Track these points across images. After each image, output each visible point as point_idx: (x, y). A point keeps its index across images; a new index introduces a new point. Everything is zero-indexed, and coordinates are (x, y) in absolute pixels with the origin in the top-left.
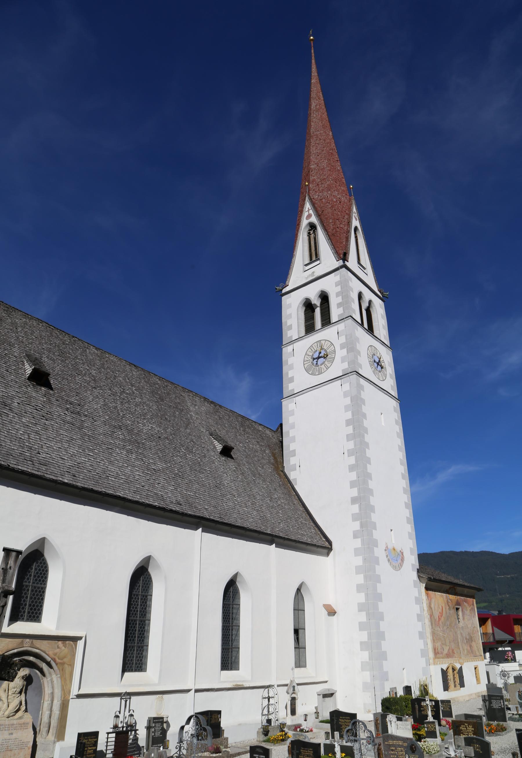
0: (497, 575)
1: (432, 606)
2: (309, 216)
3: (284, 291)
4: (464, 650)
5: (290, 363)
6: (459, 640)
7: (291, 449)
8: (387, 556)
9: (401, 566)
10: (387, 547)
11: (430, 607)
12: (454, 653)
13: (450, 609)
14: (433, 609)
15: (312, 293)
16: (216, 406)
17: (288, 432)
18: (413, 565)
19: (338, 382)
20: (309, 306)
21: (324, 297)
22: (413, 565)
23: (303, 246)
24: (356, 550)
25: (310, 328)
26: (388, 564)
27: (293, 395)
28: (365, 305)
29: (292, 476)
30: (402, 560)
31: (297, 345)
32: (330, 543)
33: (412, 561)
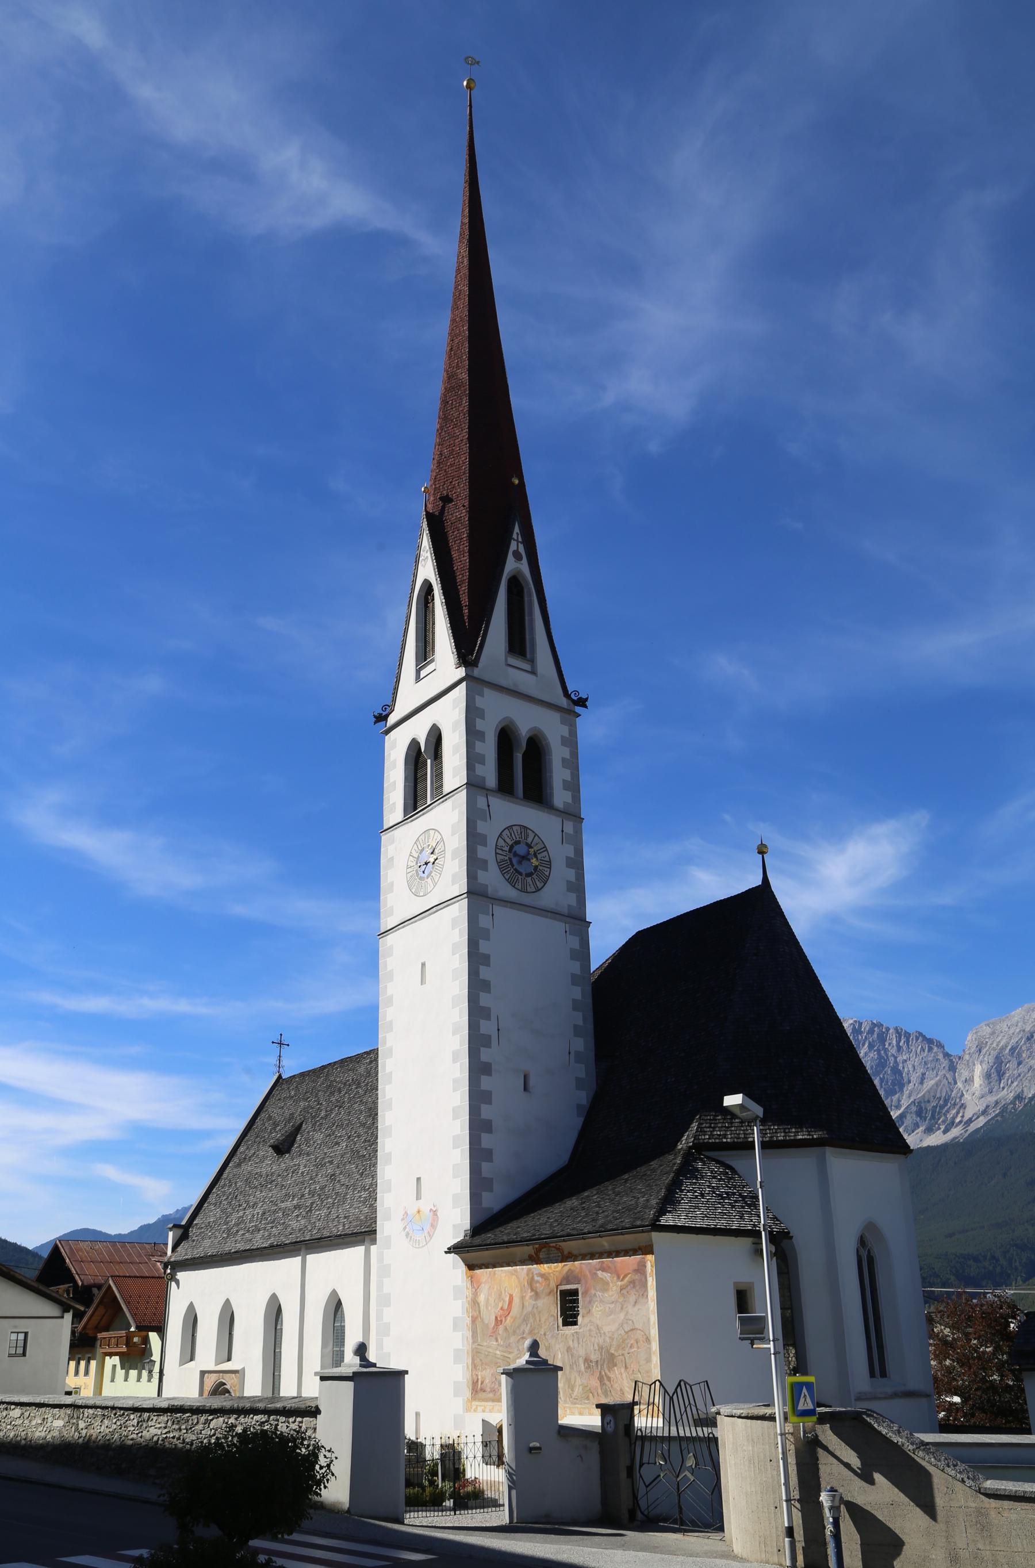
1: (482, 1298)
3: (392, 719)
13: (537, 1295)
15: (418, 729)
21: (436, 737)
30: (433, 1226)
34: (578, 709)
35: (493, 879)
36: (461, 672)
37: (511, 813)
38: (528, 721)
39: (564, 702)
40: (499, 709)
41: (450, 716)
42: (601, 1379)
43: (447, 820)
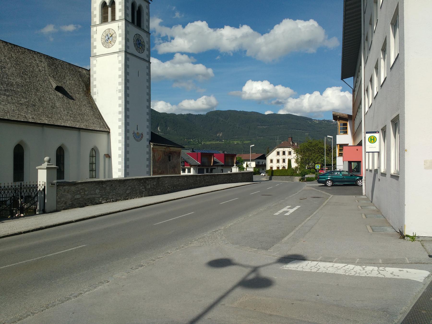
0: (259, 126)
1: (155, 155)
5: (94, 37)
7: (94, 84)
9: (141, 140)
11: (154, 156)
16: (53, 60)
19: (116, 55)
24: (119, 133)
25: (104, 19)
27: (95, 56)
28: (137, 9)
29: (94, 97)
30: (142, 137)
32: (109, 129)
33: (147, 137)
35: (133, 50)
37: (135, 30)
43: (118, 27)
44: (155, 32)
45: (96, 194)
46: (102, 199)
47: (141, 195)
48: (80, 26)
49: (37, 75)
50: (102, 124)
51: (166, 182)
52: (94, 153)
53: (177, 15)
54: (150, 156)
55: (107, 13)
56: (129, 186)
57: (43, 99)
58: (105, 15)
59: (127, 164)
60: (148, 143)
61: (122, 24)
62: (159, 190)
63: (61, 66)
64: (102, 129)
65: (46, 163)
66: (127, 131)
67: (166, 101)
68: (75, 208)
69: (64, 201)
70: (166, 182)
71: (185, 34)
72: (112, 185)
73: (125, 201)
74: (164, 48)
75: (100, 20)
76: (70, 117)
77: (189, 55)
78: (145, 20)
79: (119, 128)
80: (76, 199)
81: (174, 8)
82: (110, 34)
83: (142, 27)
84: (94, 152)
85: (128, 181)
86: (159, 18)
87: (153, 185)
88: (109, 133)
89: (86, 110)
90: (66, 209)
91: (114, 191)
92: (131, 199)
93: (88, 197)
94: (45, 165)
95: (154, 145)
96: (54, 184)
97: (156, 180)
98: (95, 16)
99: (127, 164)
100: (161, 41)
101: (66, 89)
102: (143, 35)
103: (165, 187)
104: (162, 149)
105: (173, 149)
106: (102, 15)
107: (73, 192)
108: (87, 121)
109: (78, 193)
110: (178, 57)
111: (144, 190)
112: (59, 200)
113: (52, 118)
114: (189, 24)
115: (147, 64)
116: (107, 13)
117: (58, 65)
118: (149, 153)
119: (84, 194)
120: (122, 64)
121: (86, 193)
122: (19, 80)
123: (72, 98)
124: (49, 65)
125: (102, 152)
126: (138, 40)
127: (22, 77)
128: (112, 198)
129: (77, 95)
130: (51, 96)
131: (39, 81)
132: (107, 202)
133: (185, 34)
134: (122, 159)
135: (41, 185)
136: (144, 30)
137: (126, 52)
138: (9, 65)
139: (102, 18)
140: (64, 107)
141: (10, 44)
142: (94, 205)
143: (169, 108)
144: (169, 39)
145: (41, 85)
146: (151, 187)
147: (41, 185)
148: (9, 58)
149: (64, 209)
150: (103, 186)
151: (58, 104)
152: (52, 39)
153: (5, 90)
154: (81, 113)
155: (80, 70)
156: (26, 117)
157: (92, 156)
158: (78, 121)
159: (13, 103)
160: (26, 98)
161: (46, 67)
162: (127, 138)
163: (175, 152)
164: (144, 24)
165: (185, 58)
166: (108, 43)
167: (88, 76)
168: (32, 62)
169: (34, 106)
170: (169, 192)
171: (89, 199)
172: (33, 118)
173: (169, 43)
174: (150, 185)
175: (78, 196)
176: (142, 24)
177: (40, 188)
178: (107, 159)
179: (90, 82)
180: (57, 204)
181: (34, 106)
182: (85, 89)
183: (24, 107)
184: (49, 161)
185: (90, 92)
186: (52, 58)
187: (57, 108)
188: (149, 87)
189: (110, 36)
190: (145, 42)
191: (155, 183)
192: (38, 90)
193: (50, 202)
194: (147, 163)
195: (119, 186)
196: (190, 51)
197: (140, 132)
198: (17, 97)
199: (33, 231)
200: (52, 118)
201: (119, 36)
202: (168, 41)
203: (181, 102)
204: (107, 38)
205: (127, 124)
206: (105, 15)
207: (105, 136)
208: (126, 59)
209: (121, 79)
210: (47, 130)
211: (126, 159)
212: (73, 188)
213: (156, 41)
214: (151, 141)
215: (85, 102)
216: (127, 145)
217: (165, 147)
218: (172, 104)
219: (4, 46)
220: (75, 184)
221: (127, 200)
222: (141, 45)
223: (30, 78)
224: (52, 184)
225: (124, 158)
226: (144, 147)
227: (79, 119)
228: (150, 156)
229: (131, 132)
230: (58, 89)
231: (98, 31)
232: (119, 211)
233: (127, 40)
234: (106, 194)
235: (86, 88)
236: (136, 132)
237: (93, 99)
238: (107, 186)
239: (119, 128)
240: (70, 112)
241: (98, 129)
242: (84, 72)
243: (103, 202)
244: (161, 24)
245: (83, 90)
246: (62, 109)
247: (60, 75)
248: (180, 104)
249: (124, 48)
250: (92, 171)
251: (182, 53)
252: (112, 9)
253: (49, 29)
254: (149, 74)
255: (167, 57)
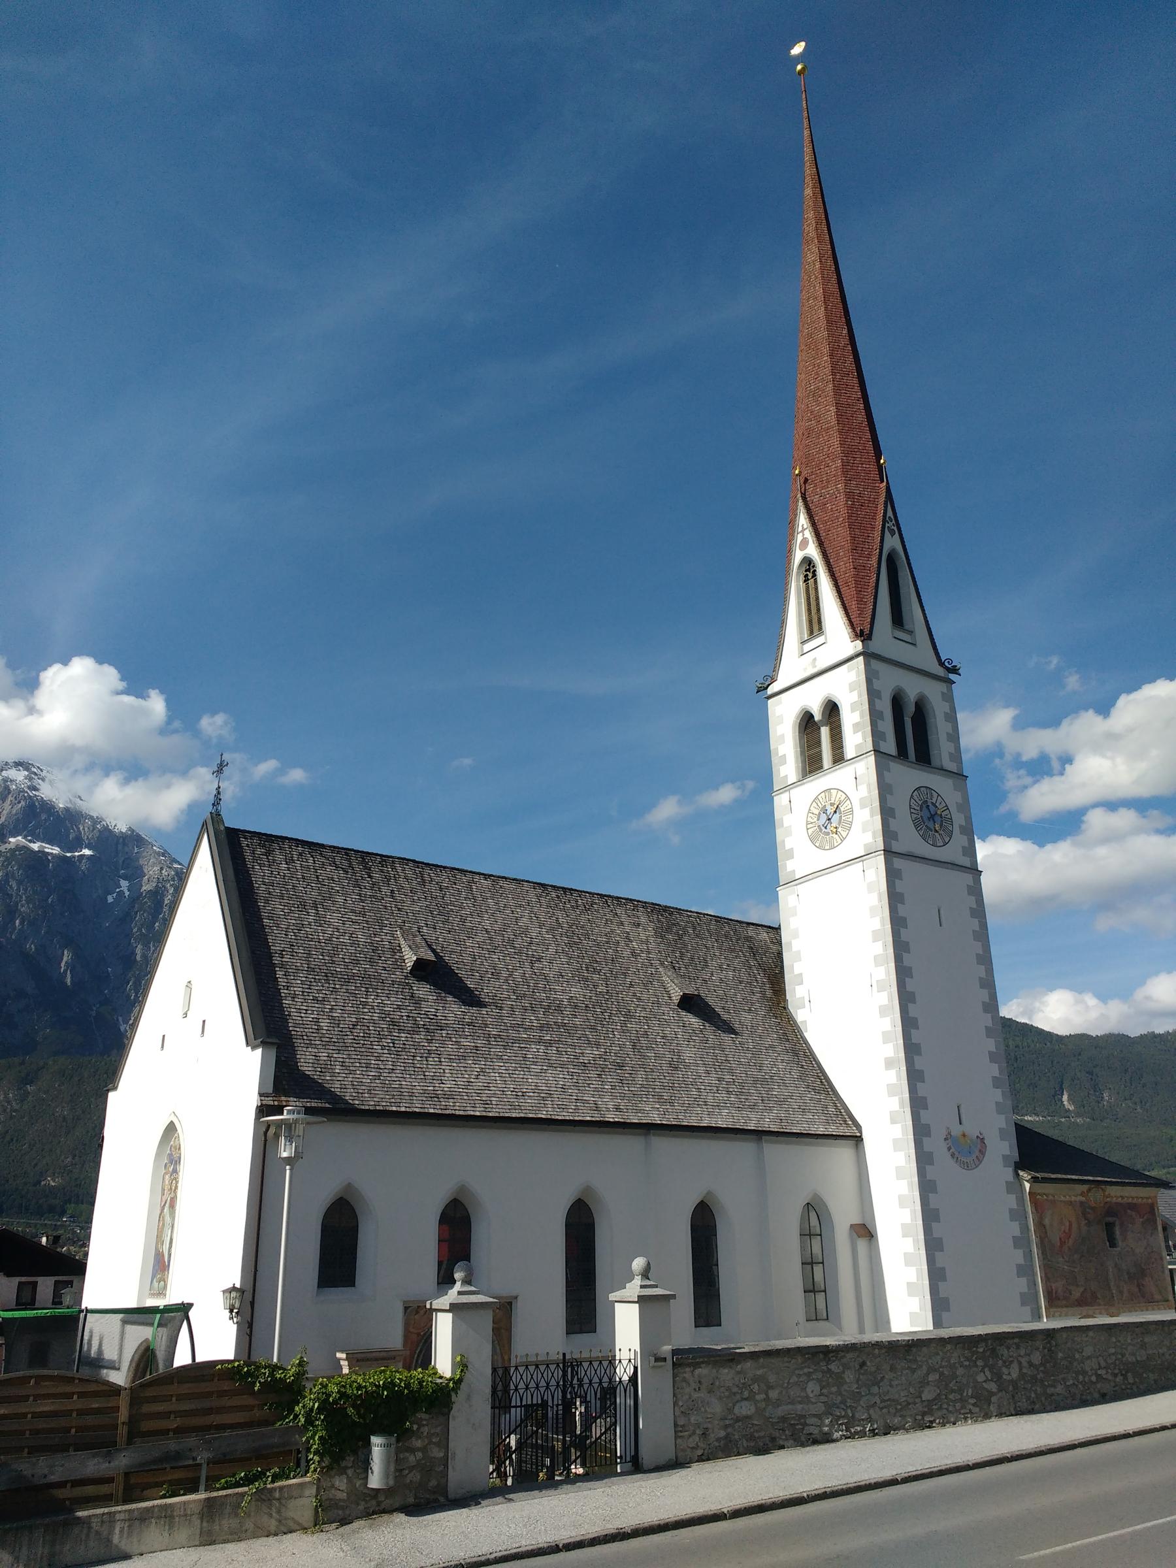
1: (1047, 1222)
2: (805, 543)
3: (770, 691)
4: (1121, 1292)
6: (1111, 1276)
8: (949, 1149)
10: (949, 1133)
11: (1040, 1225)
12: (1097, 1298)
13: (1089, 1224)
14: (1048, 1227)
15: (812, 699)
17: (790, 943)
18: (1005, 1157)
19: (858, 866)
20: (807, 723)
21: (832, 709)
22: (1005, 1157)
23: (799, 604)
24: (895, 1141)
25: (811, 764)
26: (952, 1162)
28: (910, 709)
30: (982, 1153)
31: (795, 792)
33: (1002, 1148)
34: (952, 676)
35: (910, 840)
36: (858, 646)
37: (911, 777)
38: (913, 687)
39: (941, 672)
40: (892, 679)
41: (848, 689)
42: (1138, 1286)
43: (855, 780)
44: (1001, 755)
45: (806, 1400)
46: (831, 1425)
47: (983, 1407)
48: (750, 785)
49: (628, 969)
50: (832, 1109)
51: (1089, 1350)
52: (815, 1217)
53: (1073, 681)
54: (1025, 1228)
55: (818, 743)
56: (931, 1370)
57: (643, 1041)
58: (811, 752)
59: (939, 1264)
60: (1009, 1172)
61: (867, 768)
62: (1059, 1389)
63: (694, 929)
64: (832, 1130)
65: (638, 1281)
66: (921, 1132)
67: (1078, 988)
68: (739, 1454)
69: (698, 1425)
70: (1089, 1350)
71: (1113, 738)
72: (863, 1364)
73: (919, 1434)
74: (1042, 798)
75: (797, 768)
76: (728, 1092)
77: (1140, 805)
78: (943, 737)
79: (893, 1121)
80: (738, 1420)
81: (1055, 660)
82: (832, 804)
83: (935, 761)
84: (813, 1215)
85: (925, 1349)
86: (1007, 706)
87: (1031, 1364)
88: (858, 1140)
89: (777, 1063)
90: (708, 1459)
91: (875, 1390)
92: (944, 1425)
93: (780, 1411)
94: (634, 1288)
95: (1034, 1180)
96: (665, 1359)
97: (1039, 1344)
98: (783, 760)
99: (939, 1264)
100: (1028, 780)
101: (711, 1001)
102: (942, 786)
103: (1084, 1373)
104: (1069, 1194)
105: (1117, 1194)
106: (802, 753)
107: (728, 1389)
108: (780, 1102)
109: (746, 1394)
110: (1097, 820)
111: (993, 1387)
112: (681, 1423)
113: (672, 1104)
114: (1123, 700)
115: (968, 878)
116: (819, 743)
117: (684, 929)
118: (1017, 1215)
119: (767, 1399)
120: (880, 895)
121: (773, 1394)
122: (576, 991)
123: (730, 1030)
124: (660, 934)
125: (843, 1217)
126: (925, 805)
127: (587, 980)
128: (870, 1419)
129: (746, 1017)
130: (667, 1031)
131: (631, 985)
132: (852, 1437)
133: (1113, 738)
134: (916, 1241)
135: (625, 1363)
136: (942, 769)
137: (888, 852)
138: (552, 950)
139: (804, 762)
140: (709, 1060)
141: (554, 887)
142: (803, 1445)
143: (1094, 1014)
144: (1056, 765)
145: (639, 999)
146: (1022, 1376)
147: (625, 1363)
148: (551, 930)
149: (702, 1459)
150: (833, 1367)
151: (688, 1054)
152: (676, 840)
153: (541, 1028)
154: (760, 1075)
155: (751, 932)
156: (597, 1109)
157: (807, 1234)
158: (753, 1107)
159: (562, 1066)
160: (598, 1045)
161: (651, 940)
162: (923, 1159)
163: (1132, 1207)
164: (941, 750)
165: (1125, 819)
166: (828, 834)
167: (774, 948)
168: (612, 931)
169: (621, 1066)
170: (1105, 1398)
171: (783, 1419)
172: (618, 1109)
173: (1057, 779)
174: (1015, 1365)
175: (745, 1409)
176: (934, 752)
177: (623, 1373)
178: (862, 1244)
179: (782, 967)
180: (676, 1438)
181: (621, 1066)
182: (769, 993)
183: (593, 1074)
184: (645, 1274)
185: (785, 1001)
186: (666, 909)
187: (687, 1066)
188: (985, 959)
189: (830, 810)
190: (953, 809)
191: (1036, 1358)
192: (629, 1015)
193: (657, 1429)
194: (1018, 1256)
195: (893, 1369)
196: (1143, 791)
197: (972, 1129)
198: (573, 1046)
199: (594, 1542)
200: (672, 1104)
201: (863, 806)
202: (1052, 775)
203: (1142, 982)
204: (824, 818)
205: (918, 1104)
206: (811, 752)
207: (843, 1153)
208: (892, 875)
209: (880, 944)
210: (660, 1143)
211: (933, 1246)
212: (727, 1375)
213: (1012, 780)
214: (1019, 1166)
215: (772, 1039)
216: (926, 1187)
217: (1085, 1187)
218: (1103, 998)
219: (539, 897)
220: (732, 1360)
221: (927, 1432)
222: (937, 819)
223: (607, 980)
224: (657, 1360)
225: (922, 1237)
226: (998, 1190)
227: (754, 1098)
228: (1025, 1228)
229: (938, 1133)
230: (689, 1003)
231: (796, 805)
232: (893, 1482)
233: (887, 813)
234: (843, 1402)
235: (772, 988)
236: (956, 1130)
237: (795, 1022)
238: (846, 1367)
239: (893, 1121)
240: (728, 1077)
241: (821, 1130)
242: (764, 935)
243: (836, 1435)
244: (1019, 725)
245: (763, 993)
246: (701, 1069)
247: (692, 959)
248: (1139, 994)
249: (880, 839)
250: (814, 1291)
251: (1111, 805)
252: (831, 730)
253: (667, 809)
254: (979, 911)
255: (1062, 826)
